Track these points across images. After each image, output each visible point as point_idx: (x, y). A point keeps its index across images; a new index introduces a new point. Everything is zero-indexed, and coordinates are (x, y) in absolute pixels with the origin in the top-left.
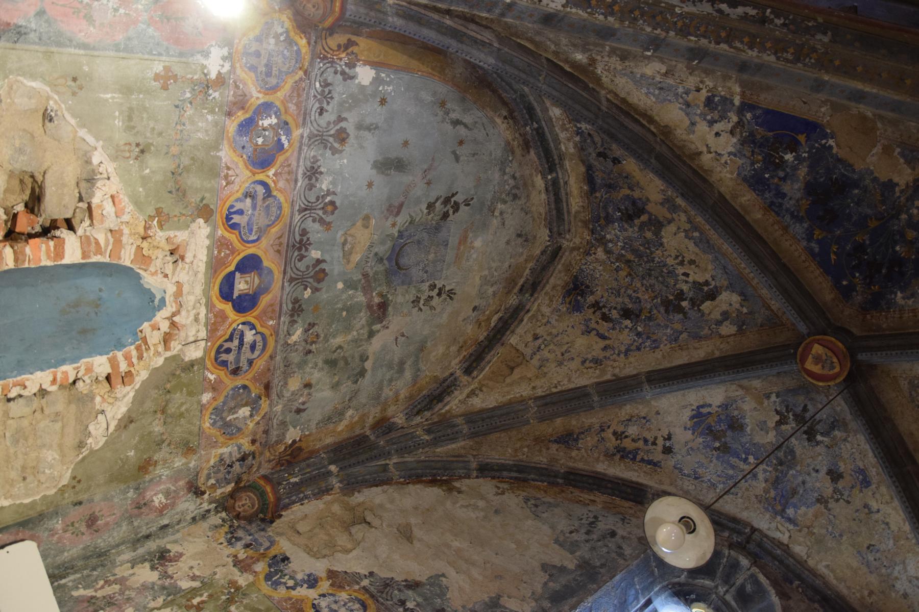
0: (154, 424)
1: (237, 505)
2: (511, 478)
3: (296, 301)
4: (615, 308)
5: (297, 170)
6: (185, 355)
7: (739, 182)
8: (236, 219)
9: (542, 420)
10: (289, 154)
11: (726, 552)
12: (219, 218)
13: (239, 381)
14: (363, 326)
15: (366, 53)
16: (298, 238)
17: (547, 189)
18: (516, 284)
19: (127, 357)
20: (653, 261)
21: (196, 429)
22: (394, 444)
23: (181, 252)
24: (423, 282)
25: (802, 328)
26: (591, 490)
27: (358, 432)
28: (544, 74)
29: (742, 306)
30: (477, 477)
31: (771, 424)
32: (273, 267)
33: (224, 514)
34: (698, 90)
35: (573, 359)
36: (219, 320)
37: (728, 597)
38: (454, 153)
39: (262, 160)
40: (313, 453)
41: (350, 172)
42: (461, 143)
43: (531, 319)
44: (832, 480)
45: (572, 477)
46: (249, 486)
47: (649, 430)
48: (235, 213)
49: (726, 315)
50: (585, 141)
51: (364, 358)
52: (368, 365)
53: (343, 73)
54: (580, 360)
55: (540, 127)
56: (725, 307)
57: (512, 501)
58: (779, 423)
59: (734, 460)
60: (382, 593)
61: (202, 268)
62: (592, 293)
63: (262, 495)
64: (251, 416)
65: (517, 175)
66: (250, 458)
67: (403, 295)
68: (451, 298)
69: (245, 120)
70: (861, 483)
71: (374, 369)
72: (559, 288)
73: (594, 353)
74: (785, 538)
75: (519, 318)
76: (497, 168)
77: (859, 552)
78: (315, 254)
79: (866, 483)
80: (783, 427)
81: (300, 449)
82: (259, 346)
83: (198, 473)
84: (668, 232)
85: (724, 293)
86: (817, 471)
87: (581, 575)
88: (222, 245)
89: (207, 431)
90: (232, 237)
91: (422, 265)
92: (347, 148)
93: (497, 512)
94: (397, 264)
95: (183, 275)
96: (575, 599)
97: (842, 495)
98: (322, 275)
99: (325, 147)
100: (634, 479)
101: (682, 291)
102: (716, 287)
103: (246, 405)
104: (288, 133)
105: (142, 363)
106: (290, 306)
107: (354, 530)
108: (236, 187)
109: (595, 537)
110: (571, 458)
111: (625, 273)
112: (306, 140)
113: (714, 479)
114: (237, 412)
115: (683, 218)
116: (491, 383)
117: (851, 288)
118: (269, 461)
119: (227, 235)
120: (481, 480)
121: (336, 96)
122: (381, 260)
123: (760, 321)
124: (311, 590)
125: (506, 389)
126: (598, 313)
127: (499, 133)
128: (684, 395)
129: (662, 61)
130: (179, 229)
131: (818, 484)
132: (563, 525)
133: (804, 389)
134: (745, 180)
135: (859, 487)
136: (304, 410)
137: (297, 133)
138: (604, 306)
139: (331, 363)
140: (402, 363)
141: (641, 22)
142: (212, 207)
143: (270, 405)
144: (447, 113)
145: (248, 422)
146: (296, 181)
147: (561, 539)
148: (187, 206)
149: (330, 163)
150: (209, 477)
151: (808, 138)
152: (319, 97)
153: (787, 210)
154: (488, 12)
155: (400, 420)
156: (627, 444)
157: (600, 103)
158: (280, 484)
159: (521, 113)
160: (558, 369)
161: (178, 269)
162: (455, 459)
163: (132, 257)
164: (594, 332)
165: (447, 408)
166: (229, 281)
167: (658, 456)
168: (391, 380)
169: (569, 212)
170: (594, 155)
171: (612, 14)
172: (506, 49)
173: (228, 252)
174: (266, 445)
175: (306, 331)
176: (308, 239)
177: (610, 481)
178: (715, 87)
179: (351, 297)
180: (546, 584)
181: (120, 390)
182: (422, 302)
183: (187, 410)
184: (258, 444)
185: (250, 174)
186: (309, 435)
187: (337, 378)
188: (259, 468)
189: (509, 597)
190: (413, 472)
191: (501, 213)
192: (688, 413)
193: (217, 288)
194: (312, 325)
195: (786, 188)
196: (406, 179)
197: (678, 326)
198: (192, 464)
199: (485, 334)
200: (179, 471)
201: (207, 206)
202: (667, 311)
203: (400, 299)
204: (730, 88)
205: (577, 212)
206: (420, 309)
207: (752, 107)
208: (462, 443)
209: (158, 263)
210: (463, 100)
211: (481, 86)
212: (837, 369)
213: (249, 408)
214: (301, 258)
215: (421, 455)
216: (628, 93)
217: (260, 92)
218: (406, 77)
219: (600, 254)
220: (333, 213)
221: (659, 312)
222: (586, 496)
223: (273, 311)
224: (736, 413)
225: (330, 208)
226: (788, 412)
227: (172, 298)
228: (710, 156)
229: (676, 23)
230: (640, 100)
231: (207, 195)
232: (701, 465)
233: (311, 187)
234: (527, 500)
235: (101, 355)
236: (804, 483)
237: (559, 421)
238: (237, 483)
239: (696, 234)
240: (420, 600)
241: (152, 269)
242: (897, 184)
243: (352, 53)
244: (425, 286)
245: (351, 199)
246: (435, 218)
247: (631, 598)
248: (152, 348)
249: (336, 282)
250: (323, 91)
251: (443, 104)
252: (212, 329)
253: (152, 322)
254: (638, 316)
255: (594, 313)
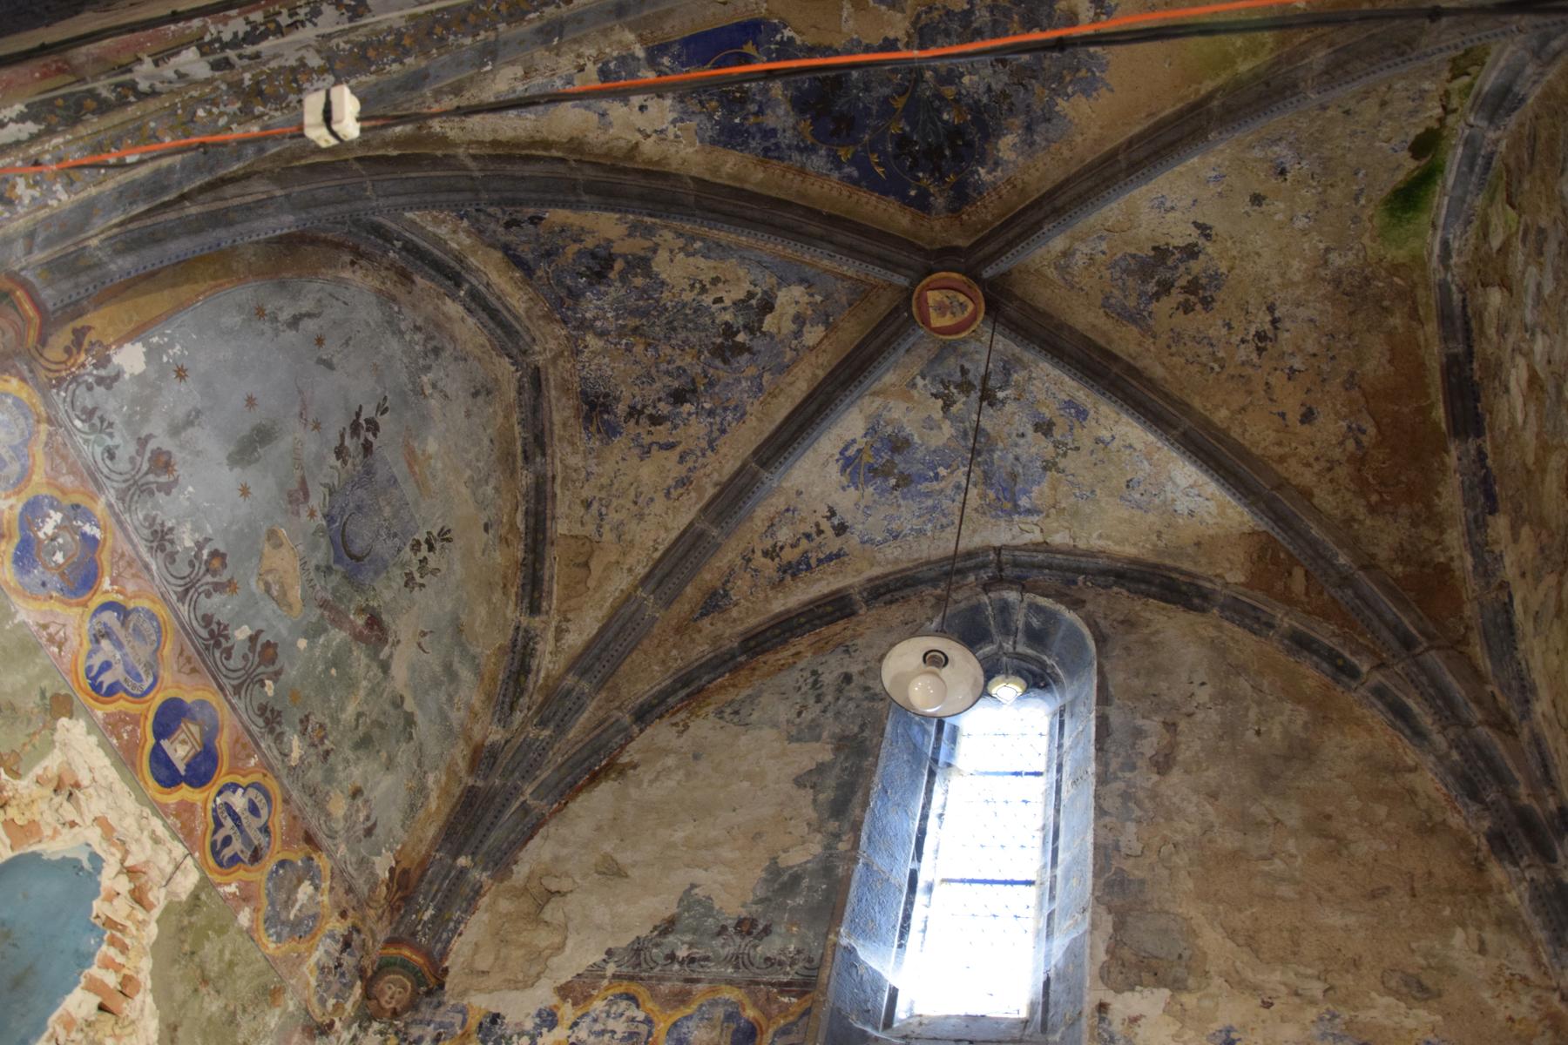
0: (206, 1005)
1: (383, 1003)
2: (682, 700)
3: (263, 710)
4: (660, 400)
5: (137, 553)
6: (177, 895)
7: (708, 148)
8: (107, 679)
9: (668, 604)
10: (113, 543)
11: (985, 599)
12: (83, 698)
13: (270, 863)
14: (368, 666)
15: (110, 330)
16: (204, 633)
17: (469, 310)
18: (515, 456)
19: (108, 964)
20: (666, 309)
21: (263, 963)
22: (513, 772)
23: (68, 780)
24: (399, 551)
25: (901, 281)
26: (786, 641)
27: (457, 791)
28: (369, 184)
29: (812, 295)
30: (642, 731)
31: (938, 415)
32: (200, 695)
33: (376, 1026)
34: (581, 69)
35: (652, 500)
36: (186, 815)
37: (1021, 649)
38: (321, 361)
39: (81, 579)
40: (424, 865)
41: (209, 496)
42: (320, 341)
43: (564, 485)
44: (1045, 434)
45: (752, 643)
46: (380, 968)
47: (803, 520)
48: (100, 673)
49: (799, 319)
50: (478, 220)
51: (398, 702)
52: (409, 705)
53: (100, 381)
54: (662, 494)
55: (407, 242)
56: (792, 310)
57: (704, 727)
58: (946, 408)
59: (924, 487)
60: (639, 964)
61: (112, 774)
62: (618, 400)
63: (405, 965)
64: (317, 888)
65: (419, 322)
66: (355, 936)
67: (388, 587)
68: (449, 540)
69: (18, 548)
70: (1077, 417)
71: (420, 704)
72: (572, 421)
73: (673, 474)
74: (1037, 536)
75: (549, 495)
76: (389, 335)
77: (1122, 498)
78: (242, 634)
79: (1082, 414)
80: (954, 409)
81: (405, 872)
82: (260, 801)
83: (306, 1010)
84: (660, 263)
85: (780, 294)
86: (1023, 435)
87: (846, 759)
88: (115, 725)
89: (278, 953)
90: (121, 705)
91: (383, 532)
92: (180, 470)
93: (696, 757)
94: (352, 557)
95: (95, 805)
96: (860, 794)
97: (1066, 445)
98: (271, 651)
99: (152, 493)
100: (826, 591)
101: (726, 323)
102: (765, 292)
103: (300, 882)
104: (89, 517)
105: (132, 954)
106: (261, 722)
107: (547, 914)
108: (74, 641)
109: (829, 698)
110: (735, 620)
111: (641, 347)
112: (119, 507)
113: (917, 523)
114: (296, 900)
115: (668, 235)
116: (573, 603)
117: (924, 194)
118: (380, 918)
119: (111, 708)
120: (649, 731)
121: (114, 418)
122: (328, 570)
123: (844, 300)
124: (556, 1031)
125: (597, 596)
126: (643, 420)
127: (356, 290)
128: (815, 450)
129: (512, 63)
130: (42, 756)
131: (1033, 450)
132: (784, 712)
133: (946, 350)
134: (713, 142)
135: (1077, 424)
136: (375, 825)
137: (99, 508)
138: (645, 407)
139: (364, 743)
140: (449, 669)
141: (452, 37)
142: (63, 692)
143: (330, 856)
144: (275, 319)
145: (319, 898)
146: (147, 567)
147: (794, 732)
148: (29, 720)
149: (168, 509)
150: (323, 1002)
151: (757, 45)
152: (92, 437)
153: (789, 147)
154: (239, 159)
155: (496, 735)
156: (789, 555)
157: (466, 168)
158: (414, 934)
159: (364, 242)
160: (643, 525)
161: (83, 803)
162: (598, 731)
163: (8, 842)
164: (655, 447)
165: (542, 674)
166: (160, 760)
167: (834, 544)
168: (450, 699)
169: (517, 318)
170: (501, 230)
171: (407, 53)
172: (297, 189)
173: (129, 728)
174: (362, 905)
175: (303, 733)
176: (219, 624)
177: (799, 615)
178: (601, 52)
179: (326, 646)
180: (815, 801)
181: (129, 1008)
182: (417, 575)
183: (233, 953)
184: (351, 913)
185: (79, 610)
186: (404, 846)
187: (384, 754)
188: (373, 934)
189: (786, 851)
190: (561, 786)
191: (434, 386)
192: (834, 469)
193: (151, 782)
194: (305, 721)
195: (770, 121)
196: (284, 444)
197: (752, 371)
198: (291, 1007)
199: (522, 546)
200: (282, 1028)
201: (56, 697)
202: (726, 361)
203: (387, 595)
204: (620, 42)
205: (527, 311)
206: (422, 585)
207: (663, 48)
208: (594, 703)
209: (49, 817)
210: (282, 285)
211: (292, 253)
212: (971, 307)
213: (307, 883)
214: (228, 653)
215: (556, 758)
216: (495, 131)
217: (7, 497)
218: (186, 317)
219: (593, 342)
220: (224, 565)
221: (717, 368)
222: (786, 654)
223: (244, 746)
224: (889, 429)
225: (216, 563)
226: (947, 388)
227: (105, 845)
228: (651, 140)
229: (497, 10)
230: (515, 129)
231: (45, 683)
232: (892, 518)
233: (172, 558)
234: (720, 714)
235: (69, 991)
236: (1017, 459)
237: (689, 590)
238: (361, 978)
239: (698, 245)
240: (688, 938)
241: (48, 832)
242: (897, 40)
243: (92, 344)
244: (407, 553)
245: (235, 528)
246: (356, 459)
247: (919, 738)
248: (129, 923)
249: (294, 644)
250: (93, 426)
251: (260, 312)
252: (186, 834)
253: (103, 894)
254: (694, 391)
255: (637, 423)
